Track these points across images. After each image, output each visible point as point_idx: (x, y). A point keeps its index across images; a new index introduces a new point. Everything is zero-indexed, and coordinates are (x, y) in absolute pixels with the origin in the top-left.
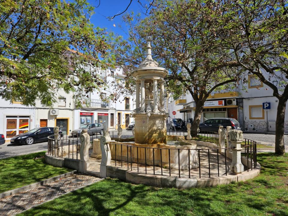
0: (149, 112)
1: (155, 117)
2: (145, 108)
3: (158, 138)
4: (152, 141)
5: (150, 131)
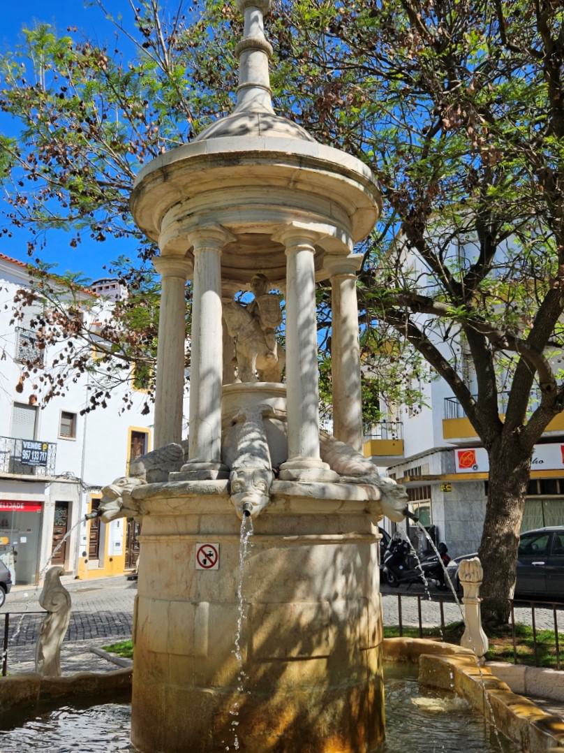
0: (253, 477)
1: (299, 516)
2: (218, 444)
3: (325, 702)
4: (278, 732)
5: (258, 640)
